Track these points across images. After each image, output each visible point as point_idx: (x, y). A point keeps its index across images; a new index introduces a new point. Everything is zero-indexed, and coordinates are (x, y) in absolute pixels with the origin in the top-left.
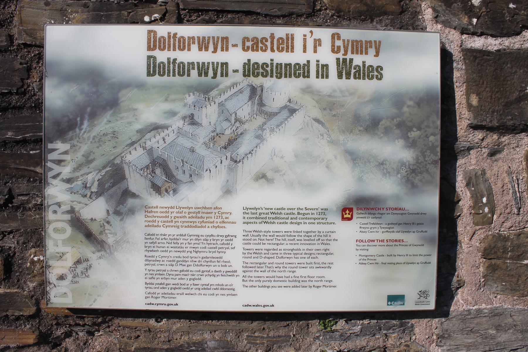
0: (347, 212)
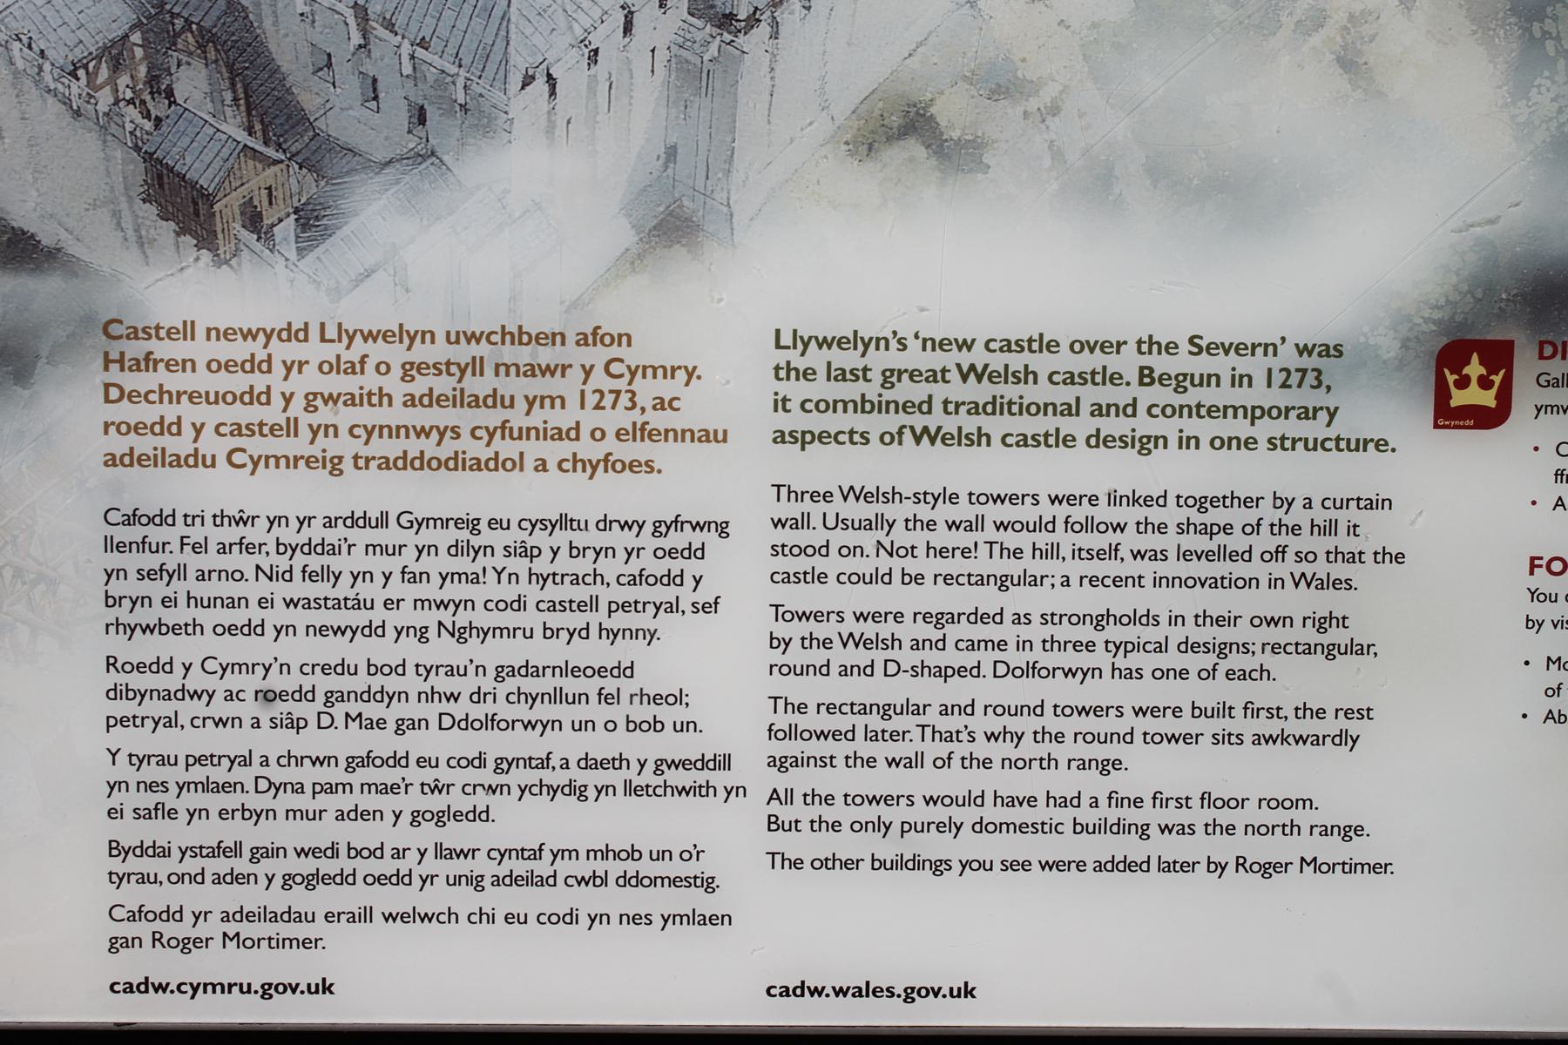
0: (1475, 369)
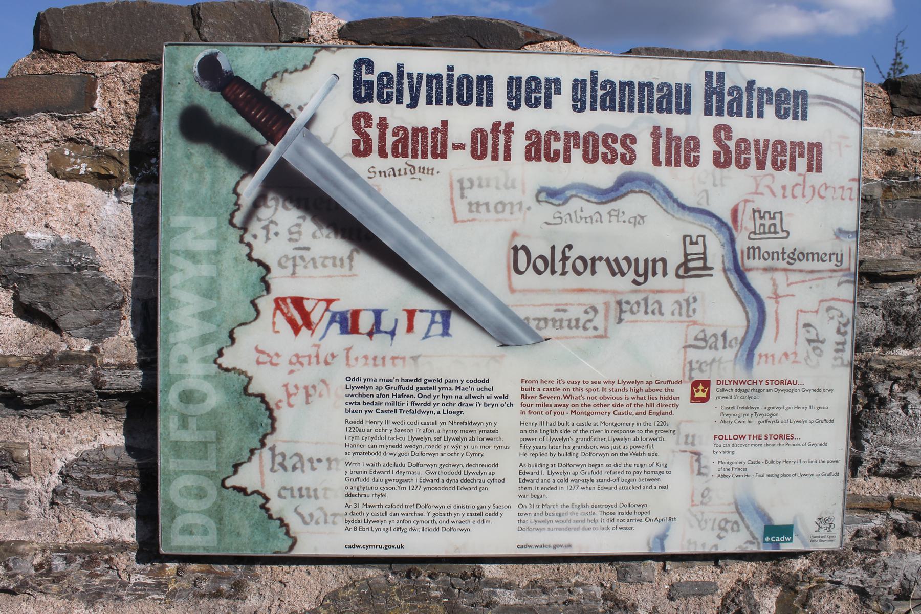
0: (701, 387)
